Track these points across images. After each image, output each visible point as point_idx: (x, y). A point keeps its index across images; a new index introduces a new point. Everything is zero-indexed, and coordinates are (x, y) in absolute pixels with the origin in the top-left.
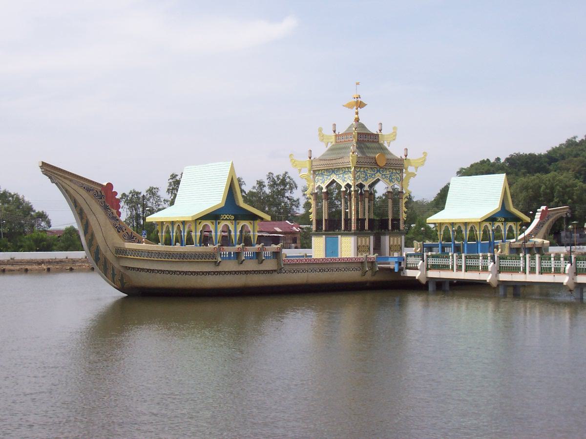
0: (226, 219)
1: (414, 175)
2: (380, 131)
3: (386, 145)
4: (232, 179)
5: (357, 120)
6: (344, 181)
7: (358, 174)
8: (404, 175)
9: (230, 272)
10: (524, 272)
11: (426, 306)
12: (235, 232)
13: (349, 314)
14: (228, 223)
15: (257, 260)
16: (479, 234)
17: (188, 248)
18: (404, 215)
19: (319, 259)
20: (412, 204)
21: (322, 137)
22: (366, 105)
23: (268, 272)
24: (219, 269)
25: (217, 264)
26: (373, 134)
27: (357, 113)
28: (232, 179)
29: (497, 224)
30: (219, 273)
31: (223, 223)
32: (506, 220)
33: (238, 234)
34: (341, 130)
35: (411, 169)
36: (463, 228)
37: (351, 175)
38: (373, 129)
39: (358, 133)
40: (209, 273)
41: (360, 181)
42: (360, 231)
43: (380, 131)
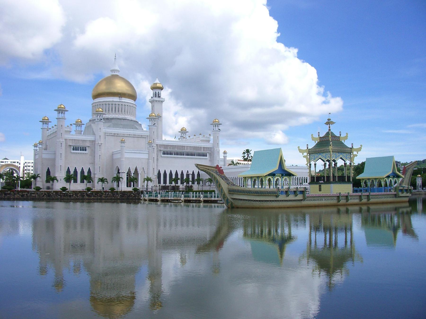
1: (356, 156)
3: (343, 141)
6: (325, 158)
9: (283, 201)
10: (76, 181)
14: (279, 177)
15: (302, 195)
16: (383, 184)
18: (353, 174)
20: (315, 177)
21: (313, 139)
23: (299, 200)
24: (278, 199)
25: (277, 196)
26: (336, 137)
27: (329, 127)
29: (390, 179)
30: (278, 201)
31: (277, 178)
32: (394, 177)
35: (355, 153)
36: (368, 181)
40: (273, 201)
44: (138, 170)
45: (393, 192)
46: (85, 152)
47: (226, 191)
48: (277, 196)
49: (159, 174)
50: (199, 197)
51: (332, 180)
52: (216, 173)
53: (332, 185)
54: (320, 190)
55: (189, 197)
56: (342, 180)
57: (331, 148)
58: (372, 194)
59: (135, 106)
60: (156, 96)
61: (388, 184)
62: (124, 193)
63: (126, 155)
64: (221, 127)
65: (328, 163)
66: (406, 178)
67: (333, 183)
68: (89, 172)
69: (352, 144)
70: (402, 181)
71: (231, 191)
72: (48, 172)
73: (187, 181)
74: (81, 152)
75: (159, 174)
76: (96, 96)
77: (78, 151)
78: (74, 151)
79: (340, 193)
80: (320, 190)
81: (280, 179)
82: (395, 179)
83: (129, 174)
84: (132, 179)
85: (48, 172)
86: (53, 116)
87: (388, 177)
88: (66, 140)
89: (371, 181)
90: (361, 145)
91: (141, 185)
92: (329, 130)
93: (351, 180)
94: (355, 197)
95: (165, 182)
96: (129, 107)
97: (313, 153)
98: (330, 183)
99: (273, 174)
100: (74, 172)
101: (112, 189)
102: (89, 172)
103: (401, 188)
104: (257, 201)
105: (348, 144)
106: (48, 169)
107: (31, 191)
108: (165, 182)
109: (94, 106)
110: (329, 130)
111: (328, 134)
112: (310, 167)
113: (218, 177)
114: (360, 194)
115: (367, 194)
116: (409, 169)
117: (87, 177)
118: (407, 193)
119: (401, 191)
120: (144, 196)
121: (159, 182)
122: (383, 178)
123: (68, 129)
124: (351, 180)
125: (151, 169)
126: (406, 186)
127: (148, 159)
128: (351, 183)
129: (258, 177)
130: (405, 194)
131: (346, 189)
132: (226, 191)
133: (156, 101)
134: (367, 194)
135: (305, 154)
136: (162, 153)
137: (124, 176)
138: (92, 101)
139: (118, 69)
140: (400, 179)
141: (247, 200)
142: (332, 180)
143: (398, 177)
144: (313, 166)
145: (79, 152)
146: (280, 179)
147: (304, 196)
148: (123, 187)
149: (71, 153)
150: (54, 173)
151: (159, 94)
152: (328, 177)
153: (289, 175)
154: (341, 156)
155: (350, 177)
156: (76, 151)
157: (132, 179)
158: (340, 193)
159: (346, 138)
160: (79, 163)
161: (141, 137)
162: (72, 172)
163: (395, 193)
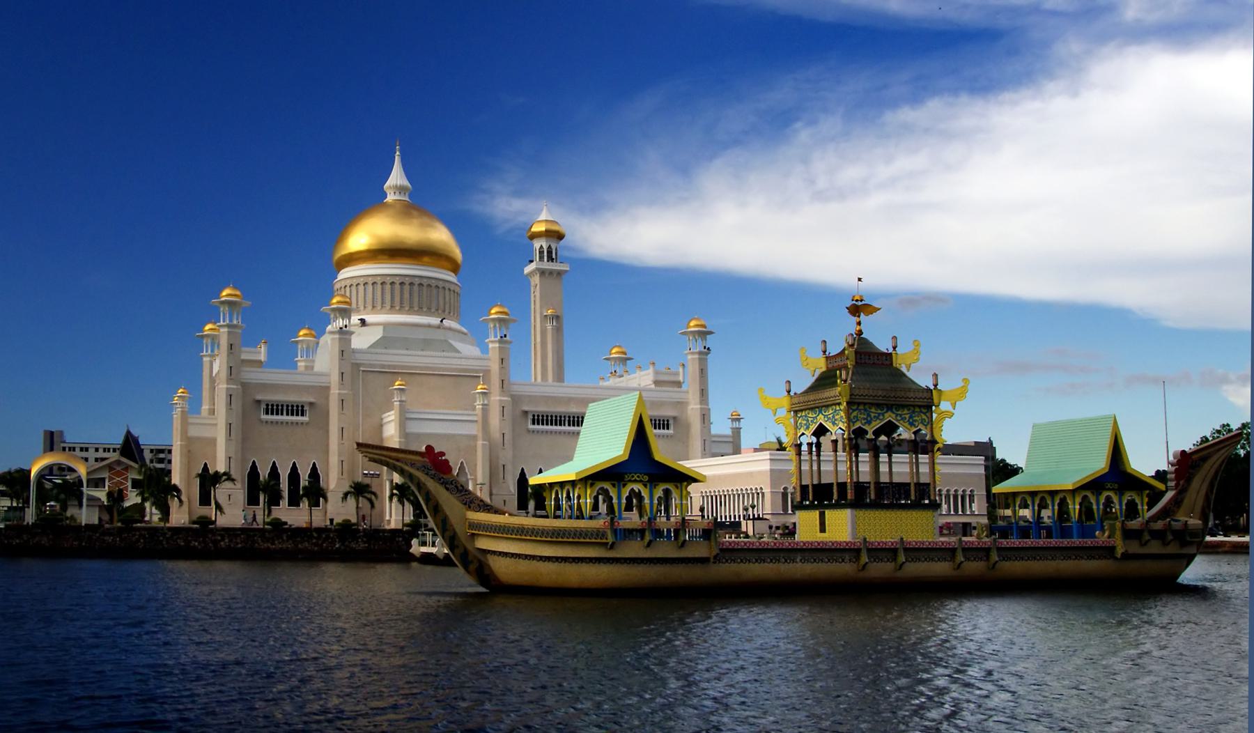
0: (635, 481)
2: (894, 348)
3: (904, 370)
4: (641, 418)
5: (860, 333)
6: (834, 424)
7: (855, 414)
8: (935, 416)
11: (992, 608)
12: (1098, 505)
13: (849, 623)
14: (637, 487)
17: (1065, 542)
19: (840, 543)
22: (129, 433)
27: (859, 323)
28: (641, 418)
31: (1106, 494)
33: (624, 501)
34: (834, 350)
35: (945, 406)
37: (842, 414)
38: (883, 345)
39: (856, 352)
41: (858, 425)
42: (27, 502)
43: (894, 348)
46: (300, 418)
51: (850, 495)
52: (424, 469)
59: (457, 289)
68: (314, 474)
69: (935, 375)
74: (290, 418)
77: (280, 417)
81: (1115, 499)
90: (935, 375)
96: (435, 291)
100: (310, 476)
101: (205, 522)
102: (314, 474)
106: (314, 467)
113: (431, 485)
129: (1053, 493)
136: (530, 421)
145: (285, 418)
149: (261, 421)
151: (550, 252)
156: (275, 417)
162: (264, 473)
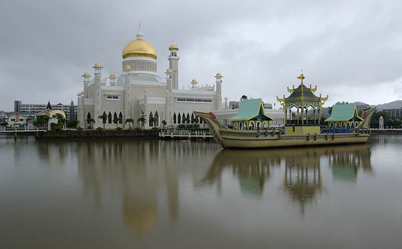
1: (324, 104)
21: (289, 90)
24: (258, 139)
29: (352, 122)
30: (258, 140)
32: (355, 121)
35: (322, 102)
38: (308, 87)
44: (158, 113)
45: (354, 133)
47: (218, 133)
48: (257, 136)
49: (175, 116)
50: (203, 135)
51: (303, 123)
53: (303, 127)
54: (294, 131)
55: (195, 134)
56: (311, 123)
57: (302, 98)
58: (335, 134)
60: (173, 55)
61: (350, 125)
62: (146, 131)
63: (149, 102)
64: (222, 79)
65: (300, 110)
66: (366, 122)
67: (304, 126)
68: (121, 115)
70: (363, 124)
71: (221, 132)
72: (89, 115)
73: (196, 120)
75: (175, 116)
76: (124, 57)
78: (109, 99)
79: (309, 134)
80: (294, 131)
82: (356, 122)
83: (151, 114)
84: (153, 120)
85: (89, 115)
86: (92, 72)
87: (351, 120)
88: (102, 90)
89: (341, 124)
91: (160, 125)
92: (302, 83)
93: (319, 123)
94: (322, 137)
95: (179, 122)
97: (289, 102)
98: (302, 126)
99: (255, 119)
102: (121, 115)
103: (361, 130)
104: (241, 140)
105: (317, 94)
107: (74, 131)
108: (179, 122)
109: (124, 64)
110: (302, 83)
111: (300, 86)
112: (286, 113)
114: (326, 134)
115: (332, 134)
116: (369, 114)
117: (118, 119)
118: (366, 133)
119: (361, 131)
120: (161, 134)
121: (175, 122)
122: (346, 122)
123: (104, 82)
124: (319, 123)
125: (168, 113)
126: (366, 126)
127: (166, 105)
128: (319, 126)
130: (364, 134)
131: (316, 130)
132: (218, 133)
133: (173, 59)
134: (332, 134)
135: (282, 102)
137: (147, 119)
138: (123, 60)
139: (143, 34)
140: (362, 122)
141: (234, 139)
142: (303, 123)
143: (360, 120)
144: (288, 111)
146: (260, 123)
147: (279, 136)
148: (147, 126)
150: (94, 117)
152: (300, 121)
153: (269, 119)
154: (311, 104)
155: (318, 120)
157: (153, 120)
158: (309, 134)
159: (315, 89)
160: (113, 108)
161: (159, 87)
163: (356, 133)
